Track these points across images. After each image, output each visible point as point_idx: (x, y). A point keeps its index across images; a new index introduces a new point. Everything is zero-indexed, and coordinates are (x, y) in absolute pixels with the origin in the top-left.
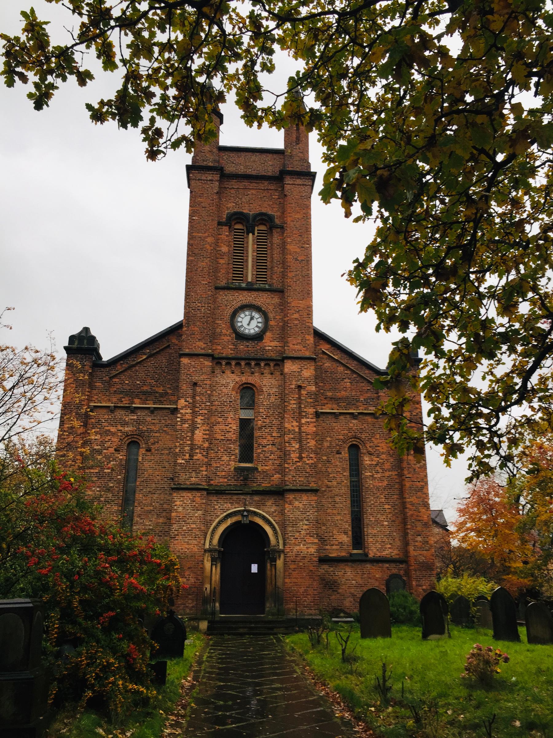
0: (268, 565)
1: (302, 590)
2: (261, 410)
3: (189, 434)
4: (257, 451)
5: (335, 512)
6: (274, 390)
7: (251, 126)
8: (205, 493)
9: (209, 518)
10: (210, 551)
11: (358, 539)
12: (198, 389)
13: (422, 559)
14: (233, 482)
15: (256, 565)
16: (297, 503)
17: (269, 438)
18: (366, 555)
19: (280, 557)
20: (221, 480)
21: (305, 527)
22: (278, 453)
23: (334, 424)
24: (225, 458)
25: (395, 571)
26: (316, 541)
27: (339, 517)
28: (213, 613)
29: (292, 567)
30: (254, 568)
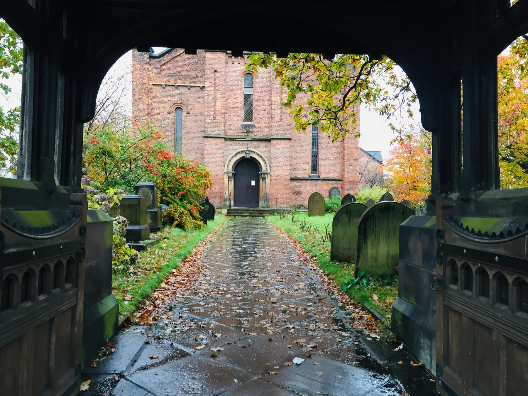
0: (261, 181)
1: (280, 195)
2: (257, 89)
3: (213, 104)
4: (255, 114)
5: (302, 151)
6: (266, 75)
8: (224, 140)
9: (226, 155)
11: (315, 168)
12: (217, 75)
13: (351, 179)
14: (240, 134)
16: (278, 146)
17: (262, 106)
18: (319, 177)
20: (233, 132)
21: (283, 160)
22: (268, 116)
23: (304, 97)
24: (235, 119)
25: (336, 186)
26: (290, 168)
27: (304, 155)
28: (230, 206)
29: (275, 182)
30: (253, 183)
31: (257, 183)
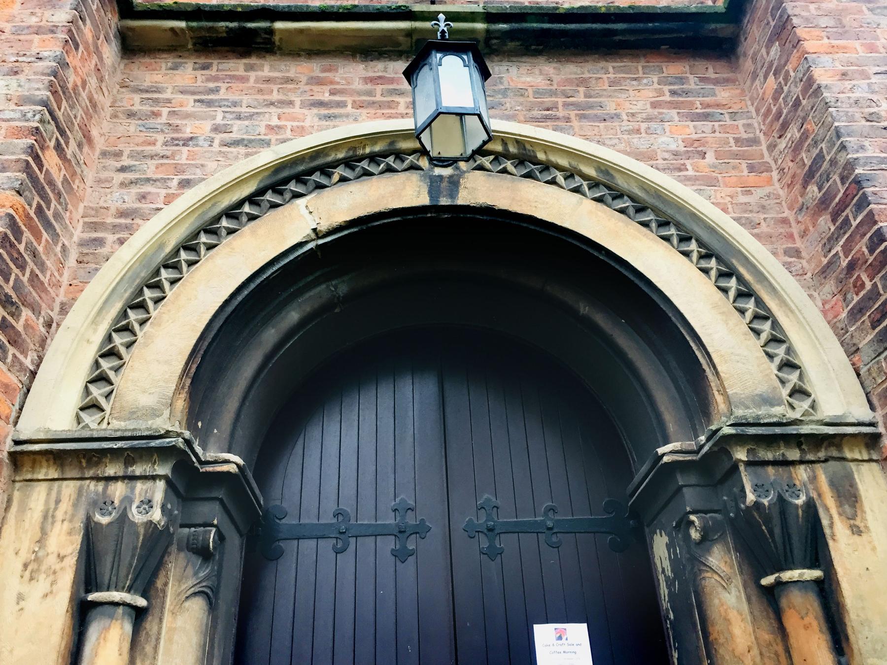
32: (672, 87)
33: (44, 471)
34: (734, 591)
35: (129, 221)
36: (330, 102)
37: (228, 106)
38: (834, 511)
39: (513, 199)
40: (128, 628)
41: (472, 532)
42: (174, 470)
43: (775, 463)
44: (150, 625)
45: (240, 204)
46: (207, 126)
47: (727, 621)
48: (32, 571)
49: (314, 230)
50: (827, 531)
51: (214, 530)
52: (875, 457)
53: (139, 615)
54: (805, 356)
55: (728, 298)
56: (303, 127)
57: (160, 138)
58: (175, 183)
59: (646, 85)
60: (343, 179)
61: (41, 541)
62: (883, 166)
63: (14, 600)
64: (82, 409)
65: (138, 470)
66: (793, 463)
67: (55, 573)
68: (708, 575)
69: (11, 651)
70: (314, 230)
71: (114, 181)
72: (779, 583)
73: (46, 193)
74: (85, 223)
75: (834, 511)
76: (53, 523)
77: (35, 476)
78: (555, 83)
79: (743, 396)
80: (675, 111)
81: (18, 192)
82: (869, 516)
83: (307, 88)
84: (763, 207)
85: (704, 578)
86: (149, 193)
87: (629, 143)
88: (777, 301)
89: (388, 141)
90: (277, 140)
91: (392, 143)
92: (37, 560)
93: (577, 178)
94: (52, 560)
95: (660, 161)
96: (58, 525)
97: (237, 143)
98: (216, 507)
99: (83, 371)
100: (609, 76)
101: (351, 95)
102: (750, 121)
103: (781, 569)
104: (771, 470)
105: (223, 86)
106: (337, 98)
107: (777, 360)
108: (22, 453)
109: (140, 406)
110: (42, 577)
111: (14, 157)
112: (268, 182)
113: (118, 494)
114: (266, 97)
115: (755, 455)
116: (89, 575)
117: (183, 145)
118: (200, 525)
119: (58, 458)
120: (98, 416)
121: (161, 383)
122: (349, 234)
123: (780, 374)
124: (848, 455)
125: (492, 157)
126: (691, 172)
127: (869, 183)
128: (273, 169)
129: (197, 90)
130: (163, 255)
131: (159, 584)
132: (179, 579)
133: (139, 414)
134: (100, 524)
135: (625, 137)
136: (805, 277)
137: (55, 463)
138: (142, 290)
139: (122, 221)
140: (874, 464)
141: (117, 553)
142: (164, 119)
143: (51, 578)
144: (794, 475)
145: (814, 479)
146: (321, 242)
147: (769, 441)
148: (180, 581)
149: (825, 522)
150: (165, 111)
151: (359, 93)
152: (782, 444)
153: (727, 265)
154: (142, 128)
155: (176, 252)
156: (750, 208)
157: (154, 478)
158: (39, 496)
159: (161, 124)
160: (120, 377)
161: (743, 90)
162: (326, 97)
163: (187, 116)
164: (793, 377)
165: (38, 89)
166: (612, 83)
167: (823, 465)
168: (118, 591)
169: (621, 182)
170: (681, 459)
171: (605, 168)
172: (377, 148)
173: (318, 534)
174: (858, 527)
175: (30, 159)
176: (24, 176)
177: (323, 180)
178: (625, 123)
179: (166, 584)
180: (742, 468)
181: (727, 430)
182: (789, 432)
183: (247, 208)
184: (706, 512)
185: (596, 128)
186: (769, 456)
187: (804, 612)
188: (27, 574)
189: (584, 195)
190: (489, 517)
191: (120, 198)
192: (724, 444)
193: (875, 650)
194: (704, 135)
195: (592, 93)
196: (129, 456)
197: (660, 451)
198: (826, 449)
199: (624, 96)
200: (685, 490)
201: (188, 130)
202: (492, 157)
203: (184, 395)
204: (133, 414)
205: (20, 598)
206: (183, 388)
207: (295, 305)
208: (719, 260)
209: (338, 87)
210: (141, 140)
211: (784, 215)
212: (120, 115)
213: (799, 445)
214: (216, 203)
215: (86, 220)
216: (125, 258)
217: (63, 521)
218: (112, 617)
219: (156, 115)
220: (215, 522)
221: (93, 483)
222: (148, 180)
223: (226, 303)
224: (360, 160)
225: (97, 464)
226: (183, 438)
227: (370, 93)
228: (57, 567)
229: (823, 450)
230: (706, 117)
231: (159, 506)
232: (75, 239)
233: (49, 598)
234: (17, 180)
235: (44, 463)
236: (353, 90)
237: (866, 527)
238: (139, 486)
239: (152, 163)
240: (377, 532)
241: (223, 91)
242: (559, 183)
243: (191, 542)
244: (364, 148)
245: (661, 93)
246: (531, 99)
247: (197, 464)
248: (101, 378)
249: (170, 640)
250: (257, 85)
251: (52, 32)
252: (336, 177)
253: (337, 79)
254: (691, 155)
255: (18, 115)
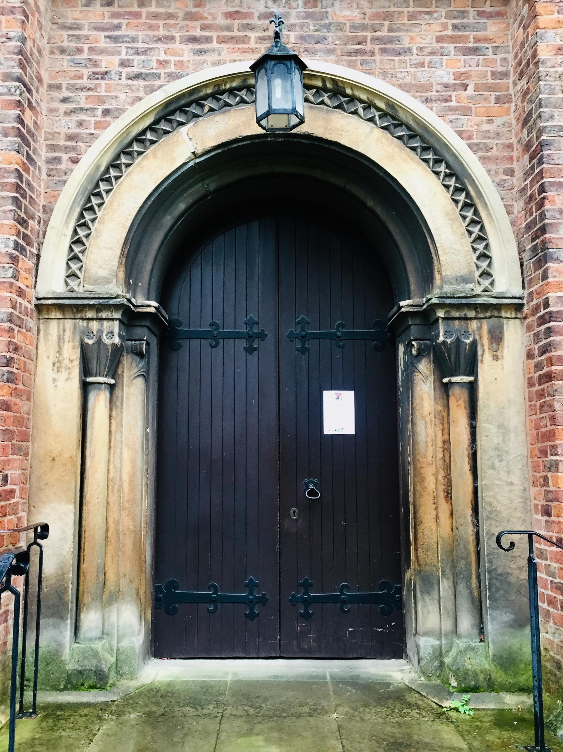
7: (250, 68)
10: (70, 308)
15: (349, 396)
19: (497, 338)
30: (339, 413)
31: (384, 413)
32: (455, 21)
33: (54, 314)
34: (428, 384)
35: (74, 144)
36: (201, 37)
37: (129, 42)
38: (486, 347)
39: (326, 128)
40: (108, 394)
41: (292, 337)
42: (123, 315)
43: (460, 319)
44: (117, 391)
45: (144, 132)
46: (116, 60)
47: (422, 399)
48: (58, 367)
49: (193, 153)
50: (479, 358)
51: (145, 343)
52: (519, 316)
53: (112, 387)
54: (494, 252)
55: (457, 207)
56: (182, 62)
57: (86, 72)
58: (99, 112)
59: (436, 19)
60: (211, 110)
61: (59, 351)
62: (561, 133)
63: (52, 382)
64: (67, 277)
65: (104, 315)
66: (471, 319)
67: (69, 368)
68: (417, 374)
69: (55, 406)
70: (193, 153)
71: (60, 111)
72: (450, 383)
73: (28, 140)
74: (47, 145)
75: (486, 347)
76: (64, 342)
77: (50, 317)
78: (367, 17)
79: (451, 277)
80: (453, 45)
81: (18, 152)
82: (506, 351)
83: (184, 23)
84: (498, 134)
85: (415, 375)
86: (84, 120)
87: (415, 76)
88: (486, 213)
89: (242, 78)
90: (165, 73)
91: (245, 80)
92: (59, 361)
93: (373, 110)
94: (66, 362)
95: (434, 93)
96: (66, 343)
97: (137, 76)
98: (146, 330)
99: (64, 255)
100: (409, 9)
101: (216, 31)
102: (506, 55)
103: (453, 375)
104: (457, 322)
105: (124, 22)
106: (206, 33)
107: (478, 253)
108: (42, 305)
109: (99, 276)
110: (63, 370)
111: (10, 125)
112: (161, 114)
113: (95, 328)
114: (155, 33)
115: (449, 314)
116: (86, 371)
117: (102, 78)
118: (137, 340)
119: (61, 308)
120: (77, 281)
121: (109, 262)
122: (216, 154)
123: (477, 262)
124: (503, 314)
125: (314, 91)
126: (453, 104)
127: (547, 147)
128: (164, 105)
129: (106, 27)
130: (100, 173)
131: (120, 371)
132: (130, 368)
133: (100, 281)
134: (89, 344)
135: (413, 70)
136: (513, 191)
137: (59, 310)
138: (89, 198)
139: (70, 143)
140: (517, 320)
141: (99, 359)
142: (85, 55)
143: (68, 371)
144: (469, 326)
145: (480, 328)
146: (198, 160)
147: (458, 307)
148: (130, 370)
149: (479, 353)
150: (86, 47)
151: (222, 28)
152: (466, 308)
153: (463, 183)
154: (72, 64)
155: (107, 171)
156: (489, 135)
157: (113, 319)
158: (54, 327)
159: (84, 59)
160: (85, 257)
161: (508, 25)
162: (198, 33)
163: (102, 52)
164: (484, 265)
165: (13, 67)
166: (411, 17)
167: (488, 320)
168: (101, 377)
169: (402, 115)
170: (412, 310)
171: (391, 104)
172: (234, 84)
173: (201, 336)
174: (498, 356)
175: (19, 126)
176: (18, 140)
177: (197, 111)
178: (415, 57)
179: (123, 372)
180: (440, 321)
181: (435, 301)
182: (470, 303)
183: (149, 136)
184: (422, 340)
185: (392, 62)
186: (457, 315)
187: (458, 399)
188: (55, 368)
189: (375, 123)
190: (303, 330)
191: (66, 125)
192: (433, 307)
193: (488, 420)
194: (470, 69)
195: (395, 27)
196: (99, 308)
197: (402, 303)
198: (491, 311)
199: (417, 30)
200: (412, 327)
201: (103, 64)
202: (314, 91)
203: (122, 269)
204: (96, 281)
205: (54, 380)
206: (121, 264)
207: (182, 198)
208: (458, 180)
209: (206, 22)
210: (73, 74)
211: (511, 141)
212: (56, 51)
213: (476, 309)
214: (129, 133)
215: (48, 142)
216: (78, 178)
217: (69, 341)
218: (100, 389)
219: (80, 51)
220: (145, 339)
221: (81, 321)
222: (82, 109)
223: (142, 207)
224: (222, 93)
225: (82, 311)
226: (127, 299)
227: (229, 28)
228: (70, 365)
229: (489, 312)
230: (475, 51)
231: (117, 335)
232: (43, 158)
233: (69, 381)
234: (16, 143)
235: (54, 310)
236: (217, 25)
237: (502, 356)
238: (105, 323)
239: (83, 94)
240: (236, 336)
241: (124, 27)
242: (360, 113)
243: (133, 349)
244: (225, 85)
245: (445, 27)
246: (348, 33)
247: (133, 309)
248: (75, 258)
249: (128, 399)
250: (148, 21)
251: (13, 13)
252: (206, 109)
253: (206, 15)
254: (457, 87)
255: (5, 90)
